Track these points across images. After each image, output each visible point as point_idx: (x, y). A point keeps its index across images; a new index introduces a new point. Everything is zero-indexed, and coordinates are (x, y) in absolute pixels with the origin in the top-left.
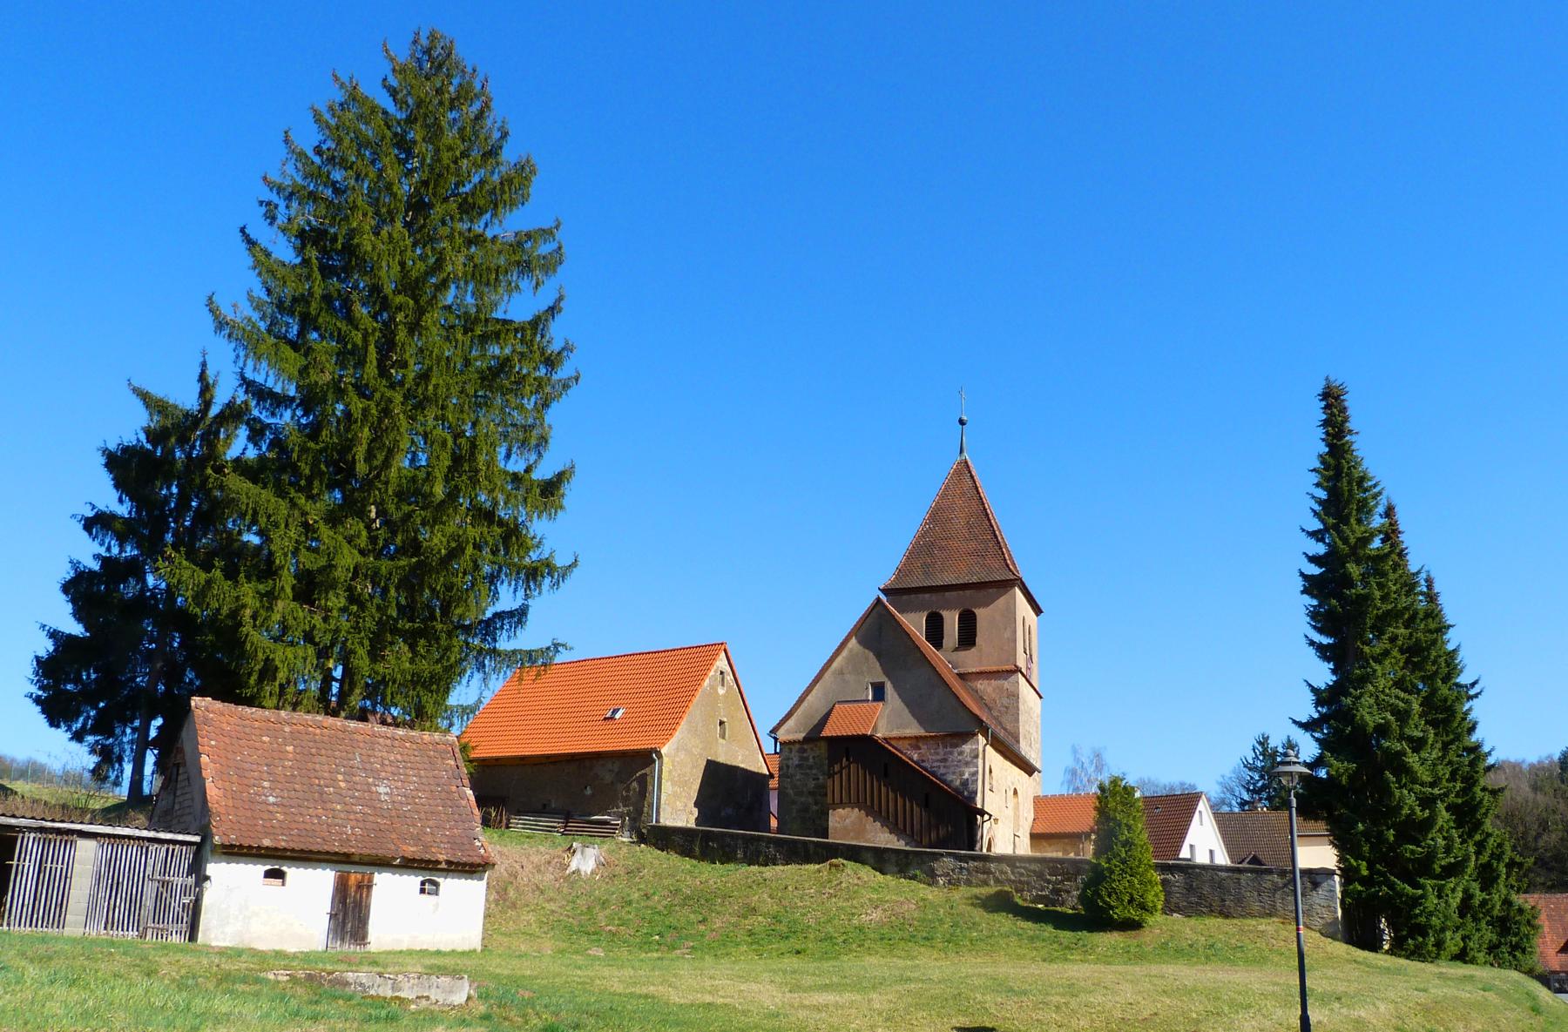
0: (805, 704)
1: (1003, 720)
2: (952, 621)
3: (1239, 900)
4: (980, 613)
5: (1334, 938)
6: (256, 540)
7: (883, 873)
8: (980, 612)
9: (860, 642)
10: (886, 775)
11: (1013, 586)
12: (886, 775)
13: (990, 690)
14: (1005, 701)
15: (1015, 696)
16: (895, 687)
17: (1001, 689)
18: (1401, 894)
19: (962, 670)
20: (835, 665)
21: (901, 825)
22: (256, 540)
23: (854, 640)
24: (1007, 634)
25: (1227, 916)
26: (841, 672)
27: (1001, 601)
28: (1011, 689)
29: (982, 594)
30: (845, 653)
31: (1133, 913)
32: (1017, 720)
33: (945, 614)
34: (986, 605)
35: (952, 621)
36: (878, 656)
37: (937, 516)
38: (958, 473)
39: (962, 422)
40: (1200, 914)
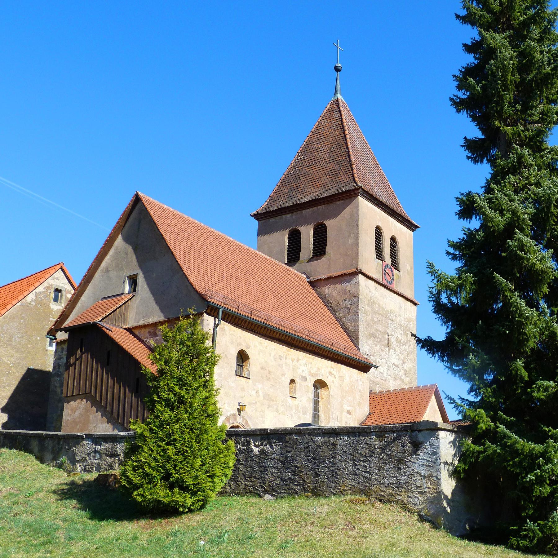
0: (79, 305)
1: (345, 321)
2: (308, 234)
3: (333, 474)
4: (329, 224)
5: (435, 526)
6: (486, 377)
7: (42, 462)
8: (328, 223)
9: (127, 240)
10: (108, 364)
11: (356, 196)
12: (108, 364)
13: (335, 293)
14: (348, 303)
15: (355, 297)
16: (146, 278)
17: (344, 291)
18: (514, 452)
19: (313, 279)
20: (104, 264)
21: (115, 415)
22: (486, 377)
23: (119, 240)
24: (351, 241)
25: (317, 494)
26: (107, 271)
27: (347, 211)
28: (352, 290)
29: (333, 206)
30: (112, 252)
31: (162, 493)
32: (357, 320)
33: (302, 229)
34: (335, 216)
35: (308, 234)
36: (135, 250)
37: (308, 149)
38: (330, 110)
39: (337, 69)
40: (292, 494)
